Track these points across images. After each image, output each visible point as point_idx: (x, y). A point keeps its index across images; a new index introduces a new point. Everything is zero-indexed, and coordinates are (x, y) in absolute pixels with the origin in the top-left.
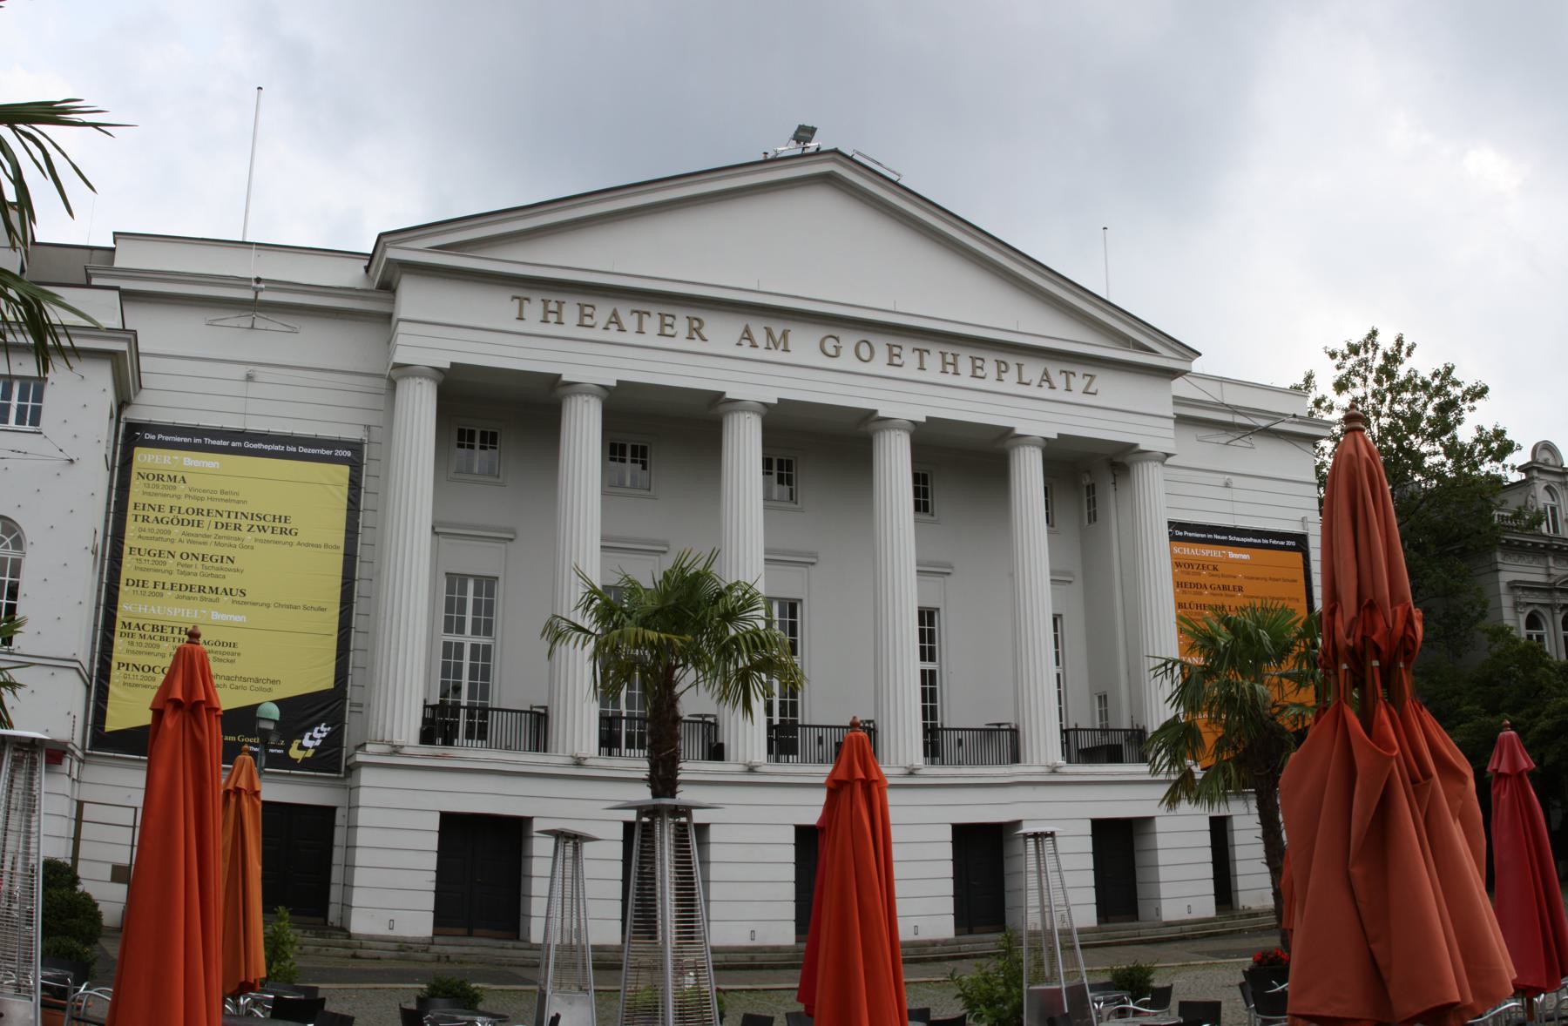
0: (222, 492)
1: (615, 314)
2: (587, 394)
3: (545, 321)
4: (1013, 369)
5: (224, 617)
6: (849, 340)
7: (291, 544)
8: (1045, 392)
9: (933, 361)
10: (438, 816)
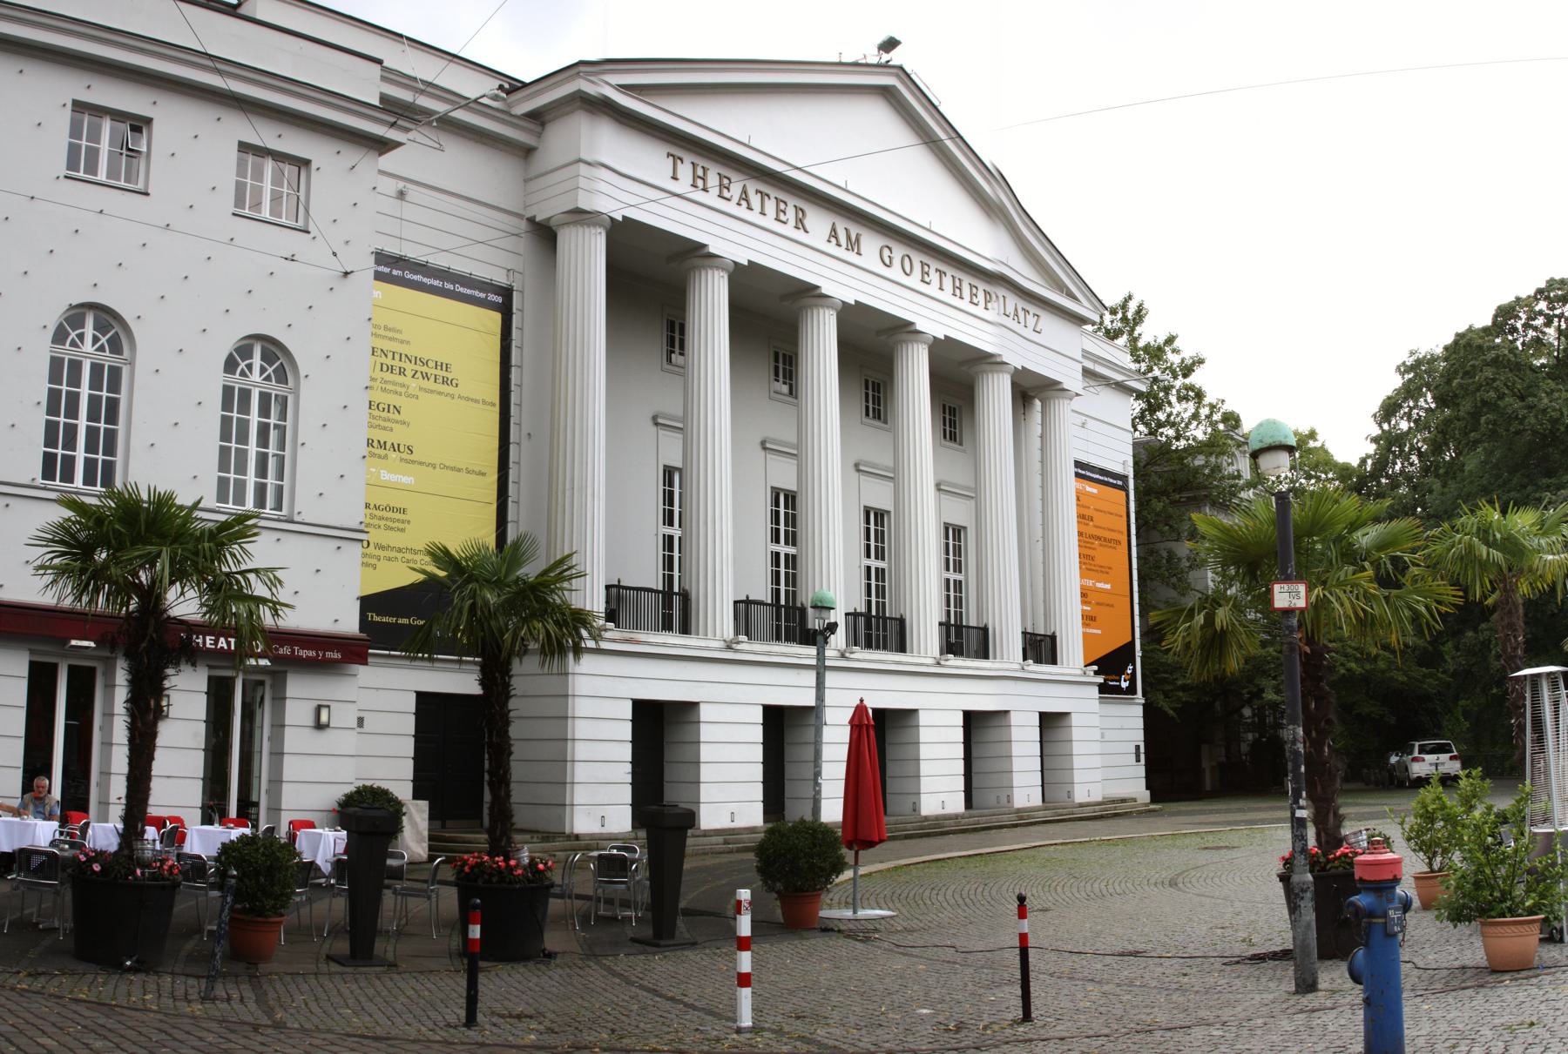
0: (386, 328)
1: (744, 191)
5: (393, 478)
6: (899, 251)
7: (452, 397)
9: (699, 181)
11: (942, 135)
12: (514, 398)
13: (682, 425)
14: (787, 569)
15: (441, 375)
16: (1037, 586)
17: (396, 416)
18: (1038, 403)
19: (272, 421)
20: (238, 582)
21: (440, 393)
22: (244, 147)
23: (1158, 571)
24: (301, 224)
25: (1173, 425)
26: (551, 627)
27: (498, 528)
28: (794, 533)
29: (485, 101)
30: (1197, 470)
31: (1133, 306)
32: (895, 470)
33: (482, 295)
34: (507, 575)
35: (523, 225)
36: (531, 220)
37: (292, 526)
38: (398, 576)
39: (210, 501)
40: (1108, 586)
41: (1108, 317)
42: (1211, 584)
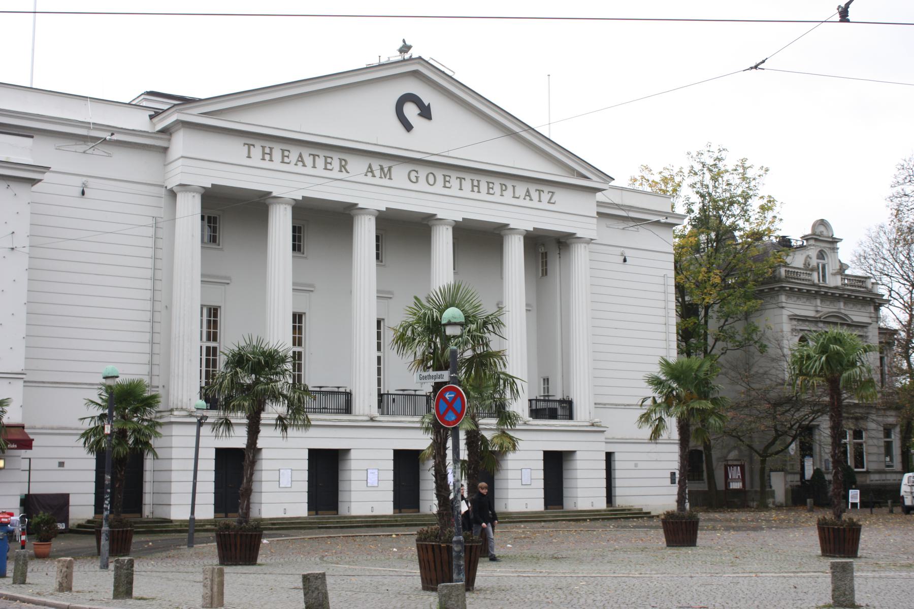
1: (300, 156)
2: (194, 192)
3: (263, 159)
4: (510, 189)
6: (423, 172)
8: (527, 203)
9: (475, 187)
10: (214, 450)
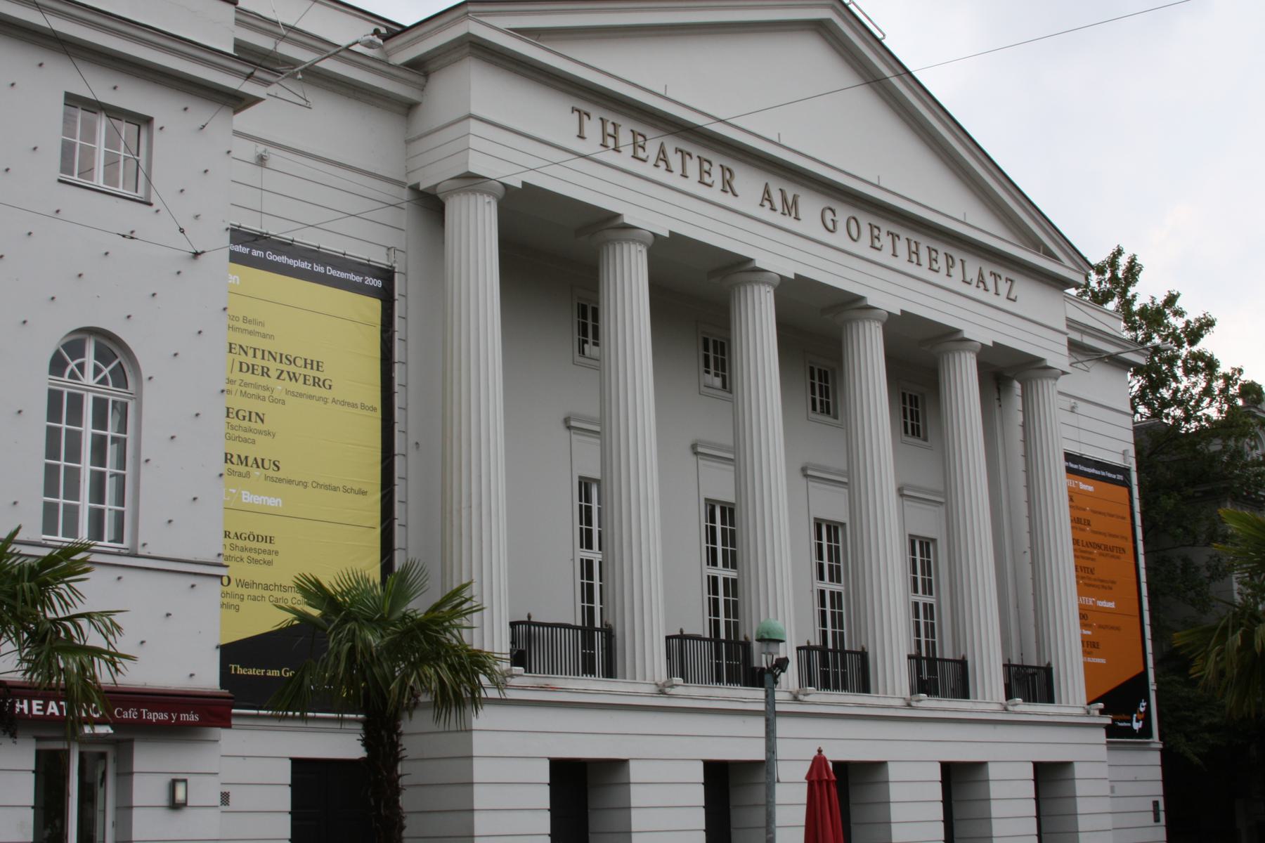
0: (245, 320)
1: (662, 150)
6: (843, 213)
7: (325, 401)
9: (609, 139)
11: (887, 72)
12: (398, 401)
13: (596, 427)
14: (726, 597)
15: (312, 375)
16: (1023, 603)
17: (259, 426)
18: (1017, 386)
19: (110, 433)
20: (67, 630)
21: (311, 397)
22: (72, 100)
23: (1173, 584)
24: (141, 194)
25: (1180, 403)
26: (446, 675)
27: (383, 558)
28: (734, 554)
29: (357, 48)
30: (1214, 457)
31: (1123, 261)
32: (849, 473)
33: (359, 279)
34: (391, 611)
35: (405, 194)
36: (415, 189)
37: (135, 560)
38: (264, 618)
39: (32, 530)
40: (1111, 605)
41: (1094, 278)
42: (1238, 598)
